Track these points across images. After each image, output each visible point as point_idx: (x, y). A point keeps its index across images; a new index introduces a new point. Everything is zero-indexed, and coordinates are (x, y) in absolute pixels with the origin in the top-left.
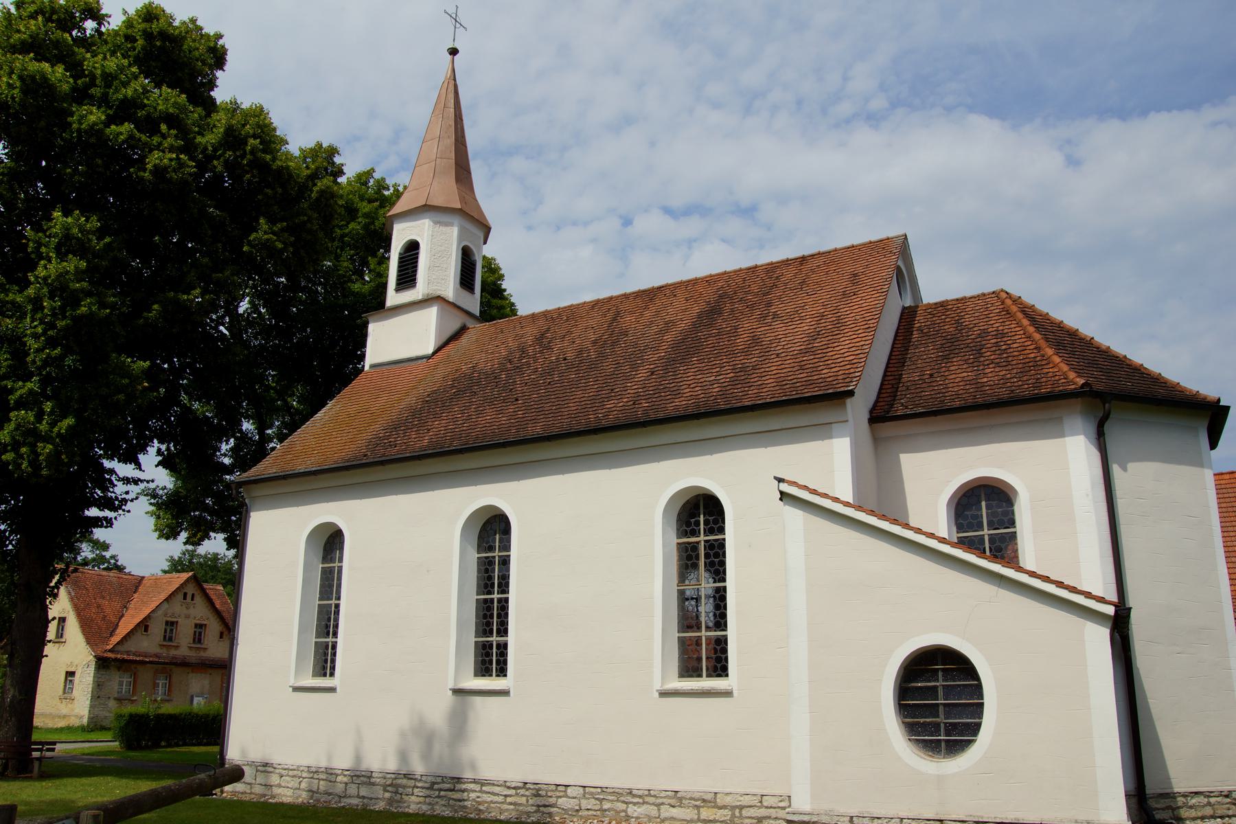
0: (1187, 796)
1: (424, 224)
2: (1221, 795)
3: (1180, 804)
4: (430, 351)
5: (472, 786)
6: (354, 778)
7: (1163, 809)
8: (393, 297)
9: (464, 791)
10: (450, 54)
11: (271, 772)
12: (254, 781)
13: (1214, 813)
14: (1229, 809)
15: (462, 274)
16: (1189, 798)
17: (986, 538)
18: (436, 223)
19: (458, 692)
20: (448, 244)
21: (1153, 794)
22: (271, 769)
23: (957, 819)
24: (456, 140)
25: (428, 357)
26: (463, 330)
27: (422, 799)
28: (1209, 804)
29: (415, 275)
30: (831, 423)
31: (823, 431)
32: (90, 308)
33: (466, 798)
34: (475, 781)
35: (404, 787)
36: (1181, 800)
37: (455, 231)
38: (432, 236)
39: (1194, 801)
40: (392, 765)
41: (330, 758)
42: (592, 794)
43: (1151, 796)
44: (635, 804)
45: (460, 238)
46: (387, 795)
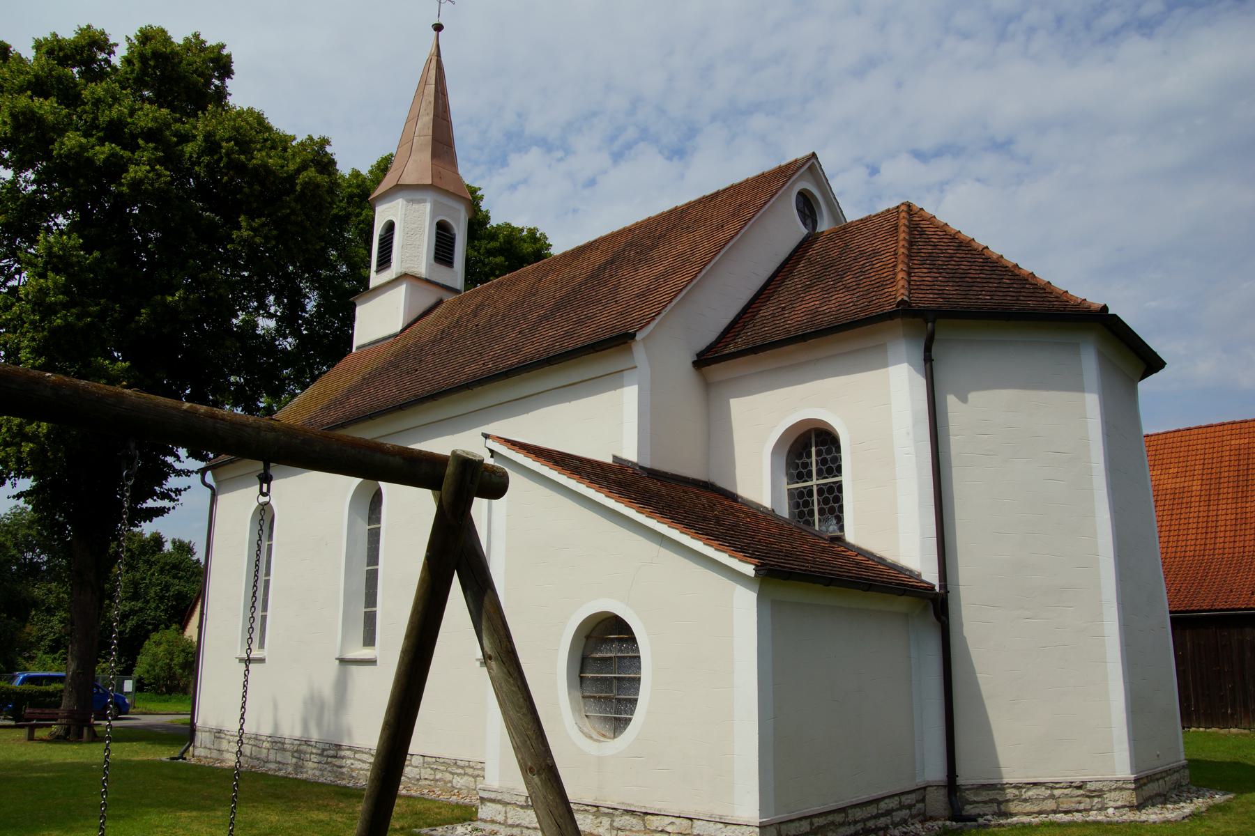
0: (1021, 787)
1: (398, 204)
2: (1070, 787)
3: (1009, 797)
4: (399, 328)
5: (347, 753)
6: (274, 744)
7: (985, 802)
8: (376, 280)
9: (343, 758)
10: (435, 30)
11: (222, 738)
12: (212, 747)
13: (1058, 807)
14: (1080, 802)
15: (436, 249)
16: (1024, 790)
17: (815, 489)
18: (408, 201)
19: (343, 661)
20: (420, 220)
21: (972, 785)
22: (223, 736)
23: (610, 806)
24: (436, 116)
25: (395, 336)
26: (439, 303)
27: (316, 765)
28: (1052, 797)
29: (390, 255)
30: (622, 371)
31: (613, 380)
32: (66, 320)
33: (344, 765)
34: (350, 749)
35: (305, 753)
36: (1011, 793)
37: (427, 208)
38: (405, 214)
39: (1030, 793)
40: (297, 733)
41: (258, 727)
42: (429, 763)
43: (970, 787)
44: (459, 775)
45: (434, 213)
46: (294, 760)
